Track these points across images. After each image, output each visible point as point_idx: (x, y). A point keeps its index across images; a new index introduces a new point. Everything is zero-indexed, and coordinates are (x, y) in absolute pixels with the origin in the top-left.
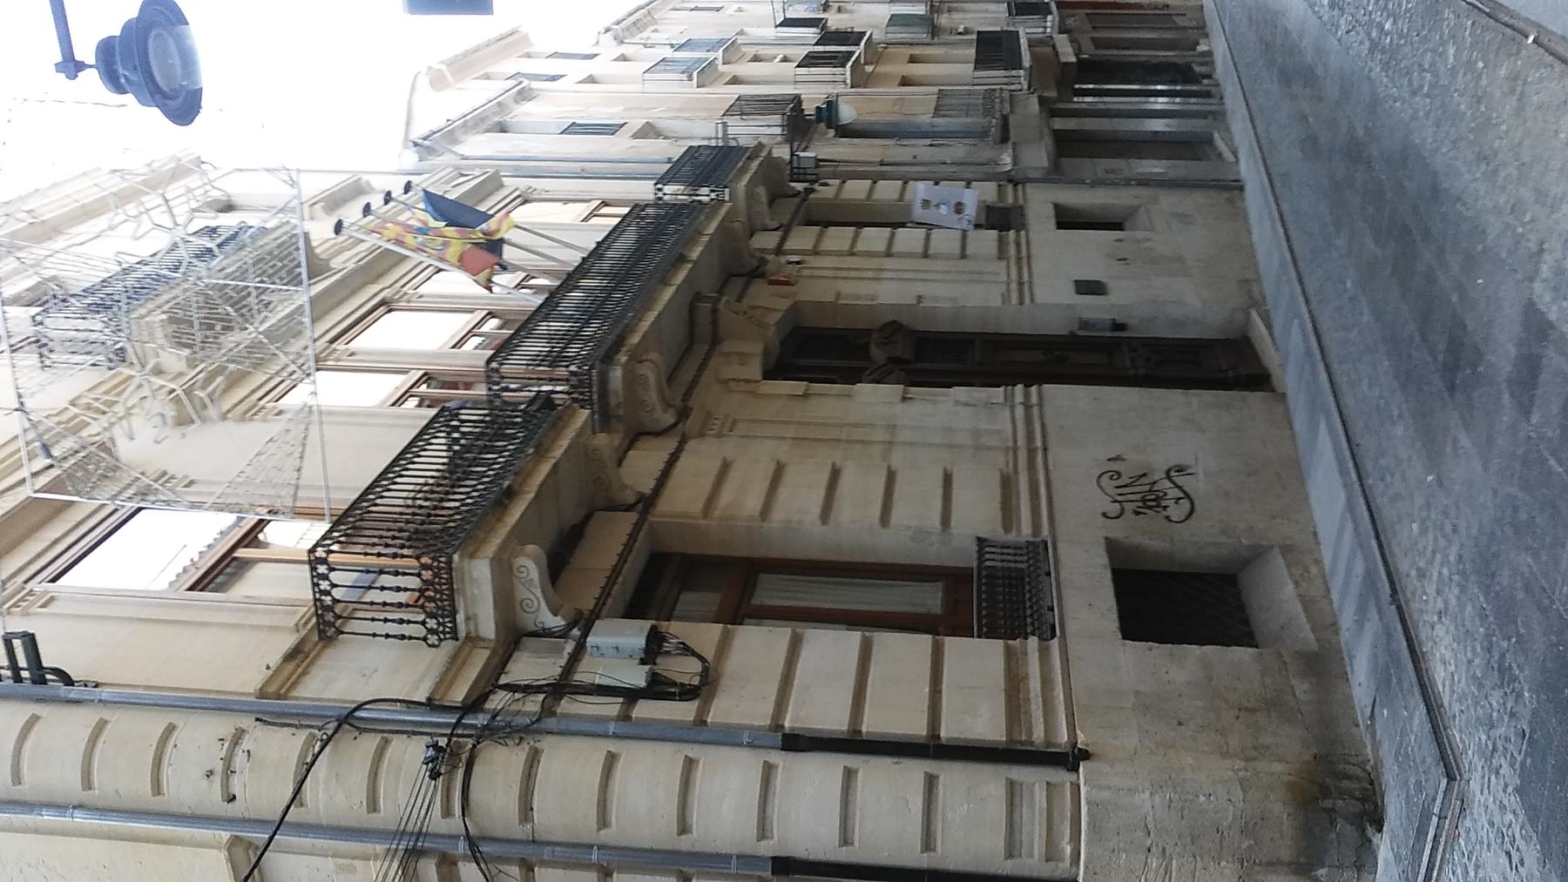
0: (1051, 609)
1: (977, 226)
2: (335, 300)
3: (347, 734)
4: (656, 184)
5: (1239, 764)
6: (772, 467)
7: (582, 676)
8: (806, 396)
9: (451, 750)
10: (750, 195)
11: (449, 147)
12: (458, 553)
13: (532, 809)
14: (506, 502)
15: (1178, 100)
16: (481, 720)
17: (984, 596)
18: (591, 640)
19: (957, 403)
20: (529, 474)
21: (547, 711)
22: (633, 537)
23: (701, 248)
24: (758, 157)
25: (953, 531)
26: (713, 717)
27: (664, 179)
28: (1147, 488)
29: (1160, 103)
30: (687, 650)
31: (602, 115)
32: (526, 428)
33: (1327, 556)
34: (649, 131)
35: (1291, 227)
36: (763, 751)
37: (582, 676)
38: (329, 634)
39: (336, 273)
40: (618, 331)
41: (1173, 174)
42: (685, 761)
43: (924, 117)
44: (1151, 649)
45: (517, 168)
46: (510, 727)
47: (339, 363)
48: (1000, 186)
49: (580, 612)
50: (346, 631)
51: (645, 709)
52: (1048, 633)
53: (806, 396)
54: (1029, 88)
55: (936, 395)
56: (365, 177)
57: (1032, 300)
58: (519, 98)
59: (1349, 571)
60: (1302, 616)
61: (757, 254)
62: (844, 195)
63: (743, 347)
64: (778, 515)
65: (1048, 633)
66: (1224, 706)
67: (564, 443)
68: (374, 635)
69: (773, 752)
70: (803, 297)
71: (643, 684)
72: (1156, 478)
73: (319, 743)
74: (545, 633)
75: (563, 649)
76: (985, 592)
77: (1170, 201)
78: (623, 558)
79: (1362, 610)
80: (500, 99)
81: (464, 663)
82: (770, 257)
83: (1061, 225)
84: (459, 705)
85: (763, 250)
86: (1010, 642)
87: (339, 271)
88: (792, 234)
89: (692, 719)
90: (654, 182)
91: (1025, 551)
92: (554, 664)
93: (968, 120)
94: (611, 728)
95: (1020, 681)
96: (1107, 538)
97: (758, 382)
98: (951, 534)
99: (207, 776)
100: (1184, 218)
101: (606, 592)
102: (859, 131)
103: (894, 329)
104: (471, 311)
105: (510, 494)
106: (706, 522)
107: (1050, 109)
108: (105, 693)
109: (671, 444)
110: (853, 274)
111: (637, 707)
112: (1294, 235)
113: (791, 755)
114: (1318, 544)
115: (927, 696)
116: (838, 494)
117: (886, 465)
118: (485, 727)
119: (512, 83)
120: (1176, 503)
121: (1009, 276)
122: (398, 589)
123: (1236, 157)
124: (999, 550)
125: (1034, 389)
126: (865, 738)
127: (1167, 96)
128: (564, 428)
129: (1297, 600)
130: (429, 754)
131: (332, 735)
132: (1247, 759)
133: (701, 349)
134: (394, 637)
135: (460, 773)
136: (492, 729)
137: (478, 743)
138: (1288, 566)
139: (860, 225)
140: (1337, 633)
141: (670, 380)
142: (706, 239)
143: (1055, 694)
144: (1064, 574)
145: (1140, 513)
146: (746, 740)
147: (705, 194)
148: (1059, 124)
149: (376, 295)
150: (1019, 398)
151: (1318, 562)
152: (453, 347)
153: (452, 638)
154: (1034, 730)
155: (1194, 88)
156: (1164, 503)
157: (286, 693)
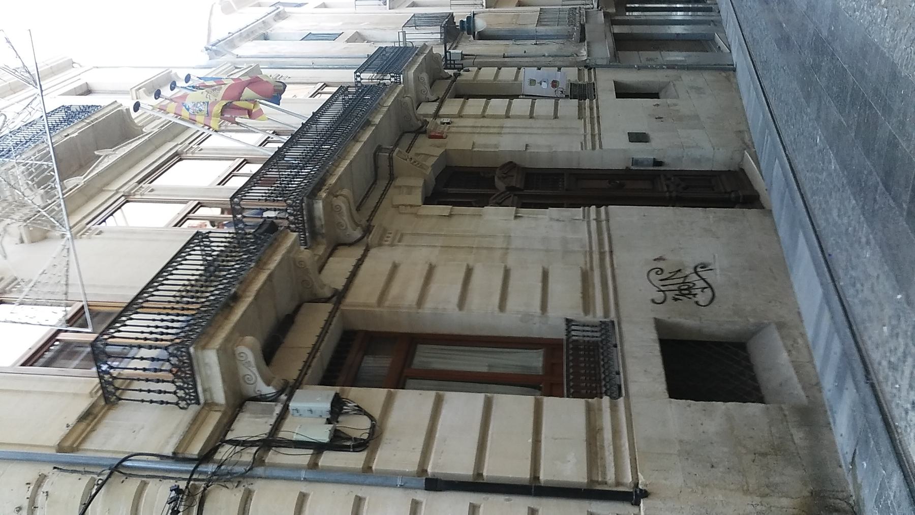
0: (618, 373)
3: (117, 478)
4: (355, 73)
5: (757, 500)
6: (427, 267)
7: (285, 433)
8: (450, 216)
9: (189, 492)
10: (417, 79)
12: (194, 346)
15: (690, 13)
16: (211, 468)
17: (571, 364)
18: (292, 405)
19: (551, 219)
21: (258, 461)
22: (328, 322)
23: (382, 116)
24: (422, 53)
26: (377, 465)
27: (361, 69)
28: (681, 280)
29: (679, 16)
30: (360, 411)
31: (328, 27)
33: (810, 334)
34: (358, 37)
35: (770, 97)
36: (411, 491)
37: (285, 433)
38: (112, 400)
39: (146, 135)
40: (322, 174)
41: (690, 61)
44: (689, 406)
45: (271, 63)
49: (286, 383)
50: (124, 398)
51: (329, 459)
52: (616, 391)
53: (450, 216)
54: (598, 7)
55: (537, 214)
56: (174, 71)
57: (601, 146)
59: (828, 348)
60: (795, 379)
61: (422, 117)
62: (480, 78)
64: (429, 305)
65: (616, 391)
66: (744, 451)
67: (277, 258)
68: (143, 401)
69: (419, 492)
70: (450, 147)
72: (687, 273)
74: (261, 398)
75: (273, 411)
76: (572, 355)
77: (688, 78)
78: (321, 337)
79: (840, 379)
80: (263, 19)
81: (202, 423)
82: (430, 120)
83: (619, 96)
84: (197, 457)
85: (426, 115)
86: (590, 400)
89: (361, 467)
92: (266, 422)
93: (559, 28)
95: (597, 432)
97: (420, 206)
100: (699, 90)
101: (307, 365)
103: (511, 167)
104: (233, 159)
105: (235, 298)
107: (611, 20)
112: (771, 101)
114: (802, 321)
116: (470, 287)
117: (503, 265)
118: (214, 474)
119: (273, 8)
125: (603, 209)
127: (684, 11)
128: (279, 246)
131: (107, 479)
132: (763, 496)
133: (382, 183)
134: (156, 402)
136: (218, 475)
137: (208, 486)
138: (782, 338)
139: (489, 97)
140: (820, 390)
141: (358, 209)
142: (385, 109)
143: (622, 442)
144: (627, 347)
146: (399, 483)
147: (388, 79)
148: (617, 29)
149: (171, 149)
150: (593, 215)
151: (803, 335)
154: (608, 472)
155: (700, 6)
156: (694, 292)
157: (78, 446)
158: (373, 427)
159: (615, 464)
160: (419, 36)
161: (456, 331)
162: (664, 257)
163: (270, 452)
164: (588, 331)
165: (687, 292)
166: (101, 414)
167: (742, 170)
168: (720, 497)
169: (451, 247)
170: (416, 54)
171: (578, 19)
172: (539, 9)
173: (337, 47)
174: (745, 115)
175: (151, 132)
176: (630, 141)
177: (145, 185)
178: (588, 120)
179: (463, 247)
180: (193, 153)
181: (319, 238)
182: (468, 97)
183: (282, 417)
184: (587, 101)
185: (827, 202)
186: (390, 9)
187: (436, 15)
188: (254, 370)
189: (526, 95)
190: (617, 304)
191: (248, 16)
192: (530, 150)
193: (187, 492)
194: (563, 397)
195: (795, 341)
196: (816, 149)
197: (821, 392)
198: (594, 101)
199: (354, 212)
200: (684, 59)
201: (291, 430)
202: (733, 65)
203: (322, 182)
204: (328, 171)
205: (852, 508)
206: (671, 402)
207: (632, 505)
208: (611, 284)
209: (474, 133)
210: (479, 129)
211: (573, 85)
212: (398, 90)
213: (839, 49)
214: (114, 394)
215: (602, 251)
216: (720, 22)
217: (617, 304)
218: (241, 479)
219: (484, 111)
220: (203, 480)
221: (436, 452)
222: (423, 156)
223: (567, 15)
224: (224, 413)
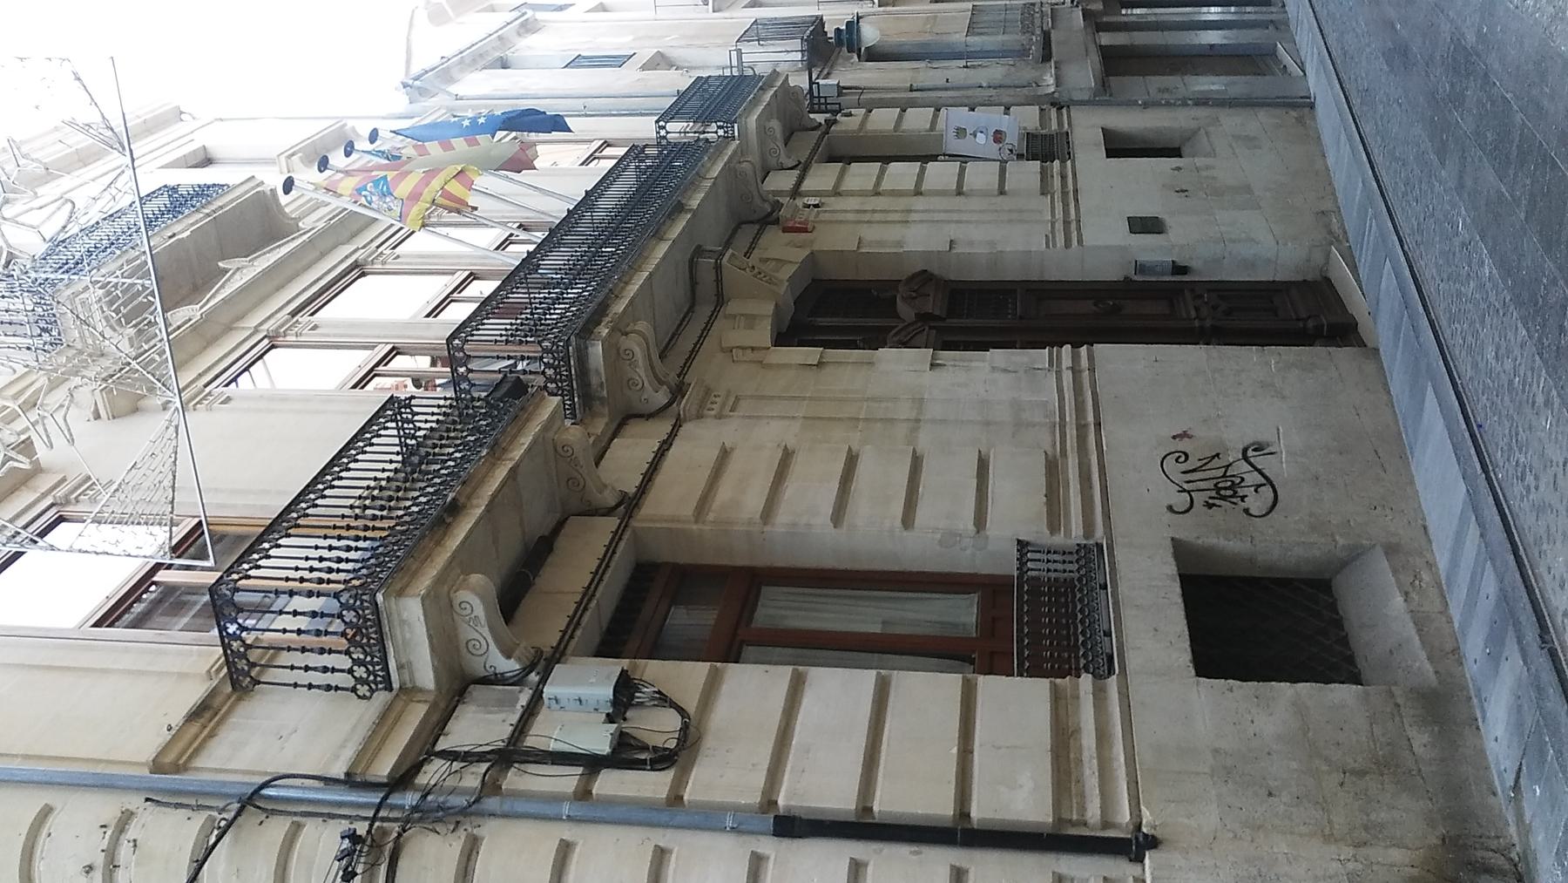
1: (1020, 157)
2: (305, 262)
3: (251, 818)
4: (657, 122)
5: (1348, 852)
8: (820, 365)
9: (373, 840)
10: (762, 129)
11: (443, 87)
14: (449, 520)
16: (409, 799)
18: (548, 691)
20: (482, 482)
21: (490, 787)
22: (611, 549)
25: (988, 533)
28: (1220, 473)
30: (663, 700)
32: (490, 416)
33: (1443, 563)
34: (660, 61)
39: (304, 233)
40: (601, 297)
42: (654, 851)
43: (957, 36)
44: (1231, 690)
46: (442, 809)
47: (299, 339)
48: (1042, 110)
49: (539, 652)
51: (610, 783)
52: (1104, 665)
53: (820, 365)
56: (350, 123)
57: (1080, 242)
58: (522, 31)
62: (870, 126)
63: (751, 307)
64: (782, 518)
65: (1104, 665)
66: (1325, 768)
67: (526, 441)
68: (296, 685)
77: (1232, 121)
78: (598, 575)
79: (1495, 640)
80: (500, 33)
82: (785, 200)
83: (1111, 153)
84: (385, 780)
87: (308, 232)
88: (811, 172)
89: (665, 796)
90: (656, 118)
91: (1076, 557)
93: (1006, 37)
94: (566, 809)
96: (1173, 539)
98: (987, 537)
99: (87, 872)
100: (1250, 142)
101: (574, 622)
102: (887, 54)
103: (924, 280)
104: (452, 273)
105: (455, 509)
106: (700, 526)
109: (663, 428)
110: (877, 217)
111: (600, 776)
112: (1378, 159)
113: (787, 844)
114: (1430, 541)
115: (955, 759)
118: (415, 809)
119: (516, 14)
120: (1256, 491)
121: (1053, 214)
123: (1303, 71)
124: (1045, 557)
125: (1084, 350)
126: (876, 821)
129: (1407, 617)
130: (344, 846)
131: (235, 818)
133: (704, 311)
134: (318, 687)
135: (383, 869)
138: (1395, 572)
139: (886, 160)
142: (708, 184)
144: (1123, 589)
145: (1214, 505)
146: (729, 823)
147: (713, 132)
148: (1106, 39)
149: (347, 257)
150: (1067, 361)
151: (1431, 565)
152: (428, 316)
153: (385, 689)
156: (1241, 492)
158: (685, 728)
161: (829, 563)
163: (509, 774)
165: (1229, 493)
166: (226, 708)
170: (761, 88)
171: (1037, 22)
172: (969, 5)
175: (313, 229)
177: (303, 318)
180: (384, 263)
181: (597, 405)
184: (1057, 163)
185: (1476, 334)
186: (714, 11)
187: (794, 20)
188: (486, 632)
189: (950, 156)
192: (958, 250)
194: (1013, 675)
198: (1069, 162)
201: (547, 734)
202: (1310, 98)
203: (603, 309)
205: (1515, 865)
206: (1198, 683)
208: (1099, 481)
211: (1030, 137)
213: (1496, 66)
214: (248, 674)
216: (1286, 23)
219: (878, 183)
220: (396, 820)
222: (774, 263)
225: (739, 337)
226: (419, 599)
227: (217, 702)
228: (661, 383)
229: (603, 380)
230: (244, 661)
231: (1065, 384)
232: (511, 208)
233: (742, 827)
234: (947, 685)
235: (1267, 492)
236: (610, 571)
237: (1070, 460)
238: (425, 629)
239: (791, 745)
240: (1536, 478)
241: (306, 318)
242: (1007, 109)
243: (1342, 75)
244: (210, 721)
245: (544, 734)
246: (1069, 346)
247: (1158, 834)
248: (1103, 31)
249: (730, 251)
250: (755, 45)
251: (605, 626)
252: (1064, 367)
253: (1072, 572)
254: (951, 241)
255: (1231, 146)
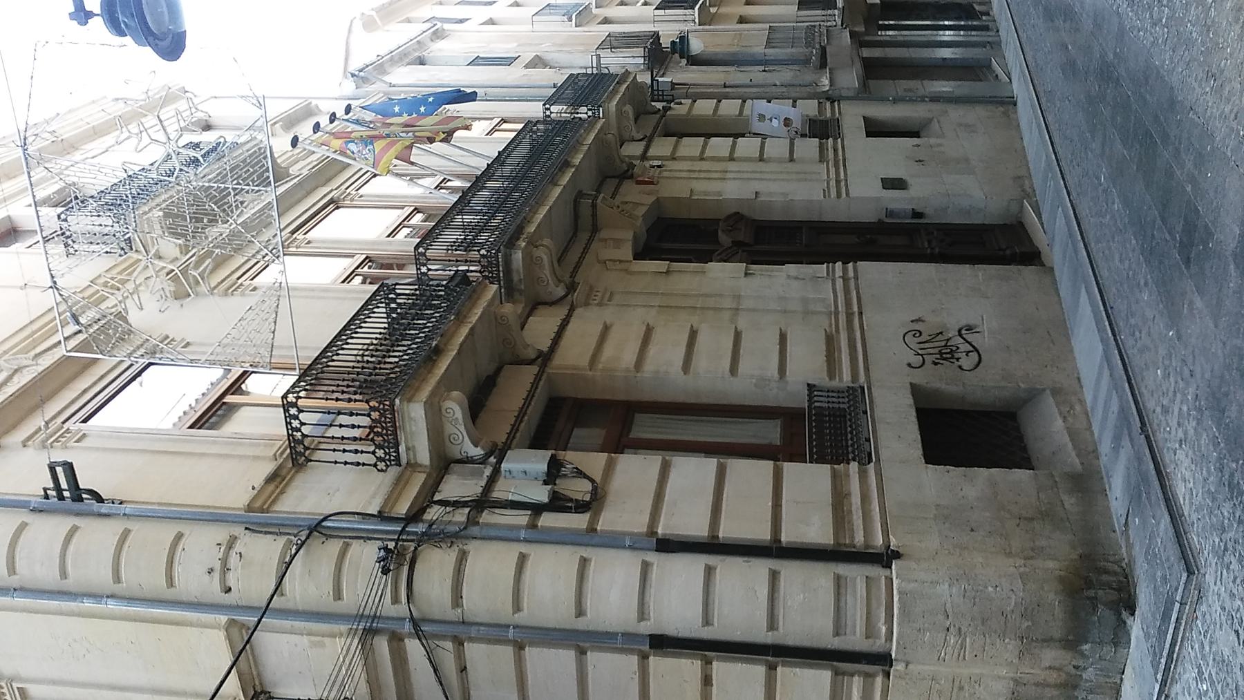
0: (869, 440)
1: (803, 136)
3: (316, 542)
5: (1020, 562)
7: (498, 494)
8: (668, 272)
10: (619, 112)
11: (380, 77)
13: (462, 597)
14: (434, 358)
15: (962, 33)
16: (420, 528)
19: (789, 277)
21: (472, 521)
24: (625, 81)
26: (602, 525)
27: (550, 101)
28: (943, 343)
29: (948, 36)
30: (580, 474)
31: (500, 50)
33: (1088, 398)
34: (538, 62)
37: (498, 494)
40: (518, 221)
47: (299, 250)
48: (819, 103)
49: (495, 445)
51: (548, 520)
52: (865, 458)
53: (668, 272)
54: (842, 25)
56: (314, 102)
57: (847, 194)
60: (1070, 445)
61: (627, 159)
64: (649, 367)
65: (865, 458)
66: (1008, 516)
67: (478, 311)
68: (336, 462)
69: (649, 553)
71: (545, 500)
73: (295, 547)
74: (468, 460)
77: (956, 114)
79: (1117, 439)
82: (637, 162)
83: (869, 134)
86: (835, 466)
93: (794, 50)
94: (523, 534)
96: (911, 384)
98: (787, 382)
99: (209, 572)
100: (970, 128)
101: (515, 428)
103: (737, 219)
104: (402, 208)
105: (438, 352)
107: (859, 41)
108: (128, 508)
109: (562, 312)
110: (703, 175)
112: (1056, 139)
113: (663, 556)
114: (1081, 387)
118: (423, 534)
119: (428, 25)
120: (967, 355)
121: (828, 177)
122: (353, 426)
125: (850, 265)
128: (478, 298)
131: (306, 539)
133: (584, 236)
135: (406, 568)
139: (708, 136)
142: (585, 148)
144: (878, 413)
145: (939, 363)
146: (628, 544)
147: (583, 113)
148: (866, 53)
149: (325, 196)
150: (839, 273)
151: (1082, 402)
153: (396, 465)
156: (956, 355)
157: (268, 508)
159: (864, 528)
160: (615, 61)
161: (681, 398)
162: (923, 319)
163: (484, 514)
164: (833, 397)
165: (948, 356)
166: (289, 476)
167: (1021, 225)
168: (980, 560)
169: (671, 307)
170: (618, 83)
171: (817, 40)
172: (767, 26)
173: (513, 75)
174: (1025, 157)
175: (300, 175)
176: (884, 188)
177: (299, 236)
178: (831, 164)
179: (684, 308)
180: (352, 200)
181: (517, 296)
182: (682, 136)
183: (492, 480)
184: (830, 140)
185: (1110, 249)
186: (576, 26)
187: (637, 34)
188: (462, 428)
189: (754, 134)
190: (867, 369)
191: (397, 35)
192: (762, 198)
193: (396, 552)
195: (1072, 407)
196: (1101, 188)
197: (1098, 459)
198: (839, 140)
199: (556, 265)
200: (951, 90)
201: (504, 490)
202: (1013, 98)
203: (520, 230)
204: (525, 218)
205: (1124, 570)
206: (926, 467)
207: (883, 567)
208: (860, 349)
209: (690, 178)
210: (697, 173)
211: (812, 122)
212: (599, 126)
213: (1124, 74)
214: (303, 454)
215: (850, 311)
216: (999, 44)
217: (867, 369)
218: (454, 540)
219: (703, 152)
220: (412, 541)
221: (666, 514)
222: (631, 205)
223: (803, 35)
224: (429, 475)
225: (609, 253)
226: (423, 404)
227: (284, 472)
228: (560, 281)
229: (522, 277)
230: (302, 446)
231: (838, 287)
232: (452, 164)
233: (636, 545)
234: (765, 467)
235: (974, 356)
236: (535, 398)
237: (842, 336)
238: (425, 424)
239: (663, 500)
240: (1140, 333)
241: (301, 237)
242: (795, 102)
243: (1036, 82)
244: (280, 483)
245: (502, 492)
246: (840, 263)
247: (901, 551)
248: (865, 47)
249: (602, 195)
250: (608, 52)
251: (532, 434)
252: (837, 276)
253: (843, 403)
254: (756, 193)
255: (955, 130)
